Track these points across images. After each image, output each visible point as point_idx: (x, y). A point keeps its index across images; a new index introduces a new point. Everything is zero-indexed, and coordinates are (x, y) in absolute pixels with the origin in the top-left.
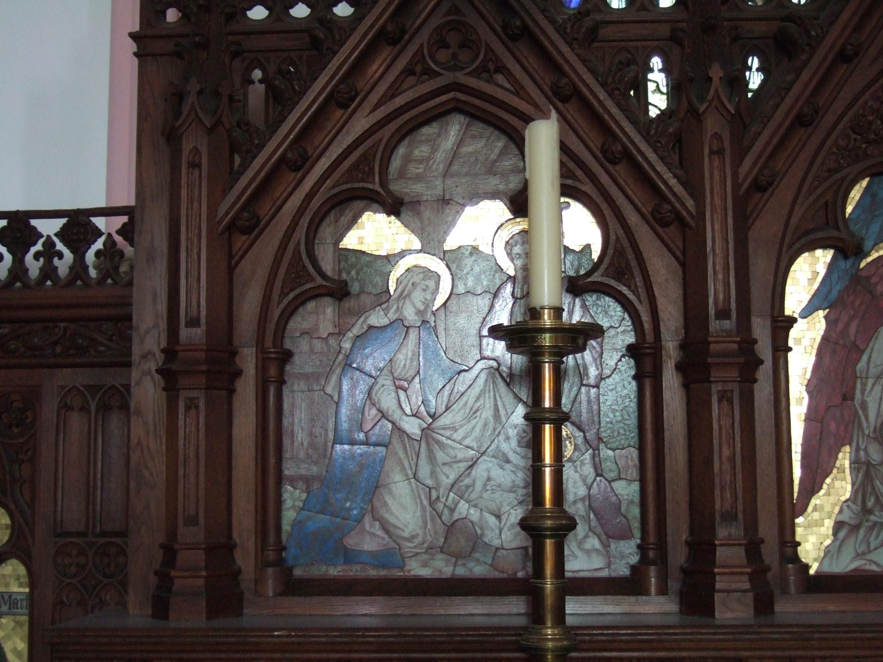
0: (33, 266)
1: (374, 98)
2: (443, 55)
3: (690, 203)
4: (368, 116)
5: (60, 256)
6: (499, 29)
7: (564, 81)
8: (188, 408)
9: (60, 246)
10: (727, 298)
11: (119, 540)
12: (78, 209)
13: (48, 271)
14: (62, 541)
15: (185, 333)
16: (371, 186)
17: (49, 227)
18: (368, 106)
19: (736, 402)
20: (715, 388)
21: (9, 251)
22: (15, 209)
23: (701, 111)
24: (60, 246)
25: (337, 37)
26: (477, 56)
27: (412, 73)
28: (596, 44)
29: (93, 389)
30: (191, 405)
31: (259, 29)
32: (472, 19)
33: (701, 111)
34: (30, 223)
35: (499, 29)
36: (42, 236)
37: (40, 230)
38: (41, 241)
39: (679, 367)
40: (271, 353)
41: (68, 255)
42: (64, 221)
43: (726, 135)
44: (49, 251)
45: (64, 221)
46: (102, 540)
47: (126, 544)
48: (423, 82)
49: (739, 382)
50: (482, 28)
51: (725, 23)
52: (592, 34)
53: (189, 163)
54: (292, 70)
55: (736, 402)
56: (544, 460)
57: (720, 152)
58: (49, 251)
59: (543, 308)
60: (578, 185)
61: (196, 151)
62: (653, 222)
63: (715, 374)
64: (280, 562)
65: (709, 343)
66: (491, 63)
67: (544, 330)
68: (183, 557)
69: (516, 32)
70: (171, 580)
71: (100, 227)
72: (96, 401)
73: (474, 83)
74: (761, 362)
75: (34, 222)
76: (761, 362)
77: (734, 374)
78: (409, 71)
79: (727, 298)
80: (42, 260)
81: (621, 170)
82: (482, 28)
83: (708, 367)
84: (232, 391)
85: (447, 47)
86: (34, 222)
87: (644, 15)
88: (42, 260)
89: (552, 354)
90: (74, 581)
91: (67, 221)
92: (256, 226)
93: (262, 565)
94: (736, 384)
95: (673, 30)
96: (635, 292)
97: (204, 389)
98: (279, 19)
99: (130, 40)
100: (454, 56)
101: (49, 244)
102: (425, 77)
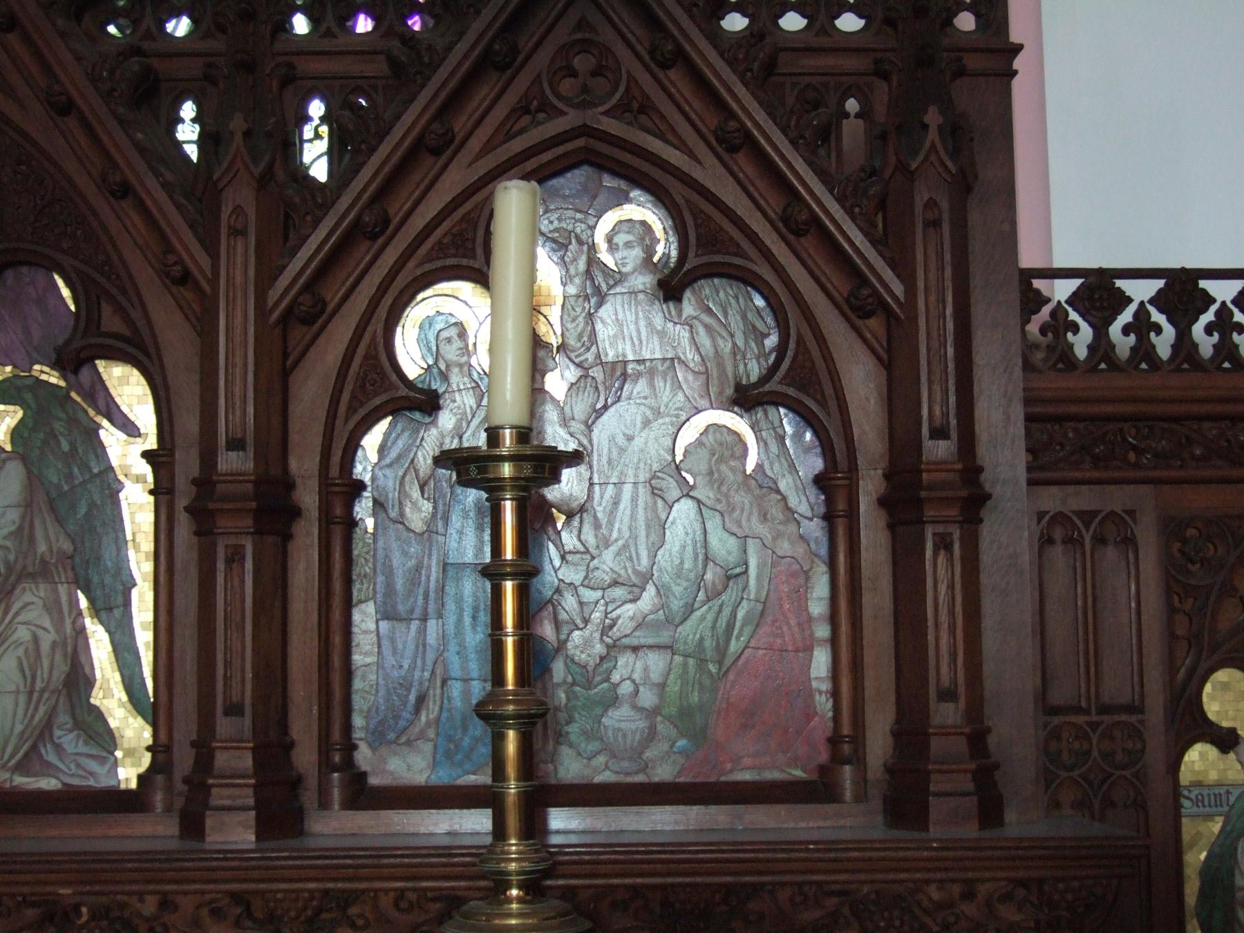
0: (1123, 343)
1: (475, 144)
2: (567, 86)
3: (898, 288)
4: (470, 164)
5: (1158, 329)
6: (643, 52)
7: (733, 124)
8: (229, 561)
9: (1157, 317)
10: (946, 415)
11: (1133, 719)
12: (1183, 270)
13: (1143, 350)
14: (1056, 720)
15: (229, 462)
16: (471, 263)
17: (1141, 291)
18: (464, 157)
19: (957, 547)
20: (929, 532)
21: (1170, 320)
22: (1179, 267)
23: (914, 165)
24: (1157, 317)
25: (426, 60)
26: (616, 89)
27: (526, 111)
28: (774, 79)
29: (1087, 516)
30: (235, 557)
31: (303, 47)
32: (607, 35)
33: (914, 165)
34: (1031, 284)
35: (643, 52)
36: (1214, 301)
37: (1212, 293)
38: (1214, 308)
39: (295, 513)
40: (336, 485)
41: (1086, 331)
42: (1160, 283)
43: (945, 205)
44: (1141, 326)
45: (1160, 283)
46: (1107, 719)
47: (1141, 722)
48: (540, 124)
49: (959, 522)
50: (622, 51)
51: (945, 54)
52: (770, 67)
53: (230, 227)
54: (364, 103)
55: (957, 547)
56: (506, 627)
57: (936, 224)
58: (1141, 326)
59: (503, 428)
60: (749, 265)
61: (238, 210)
62: (849, 312)
63: (929, 513)
64: (348, 763)
65: (921, 471)
66: (635, 102)
67: (502, 459)
68: (222, 760)
69: (667, 56)
70: (207, 789)
71: (1235, 293)
72: (1091, 533)
73: (613, 126)
74: (187, 509)
75: (1120, 283)
76: (187, 509)
77: (954, 512)
78: (523, 109)
79: (946, 415)
80: (1216, 335)
81: (809, 244)
82: (622, 51)
83: (919, 503)
84: (287, 537)
85: (574, 74)
86: (1120, 283)
87: (823, 41)
88: (1216, 335)
89: (514, 488)
90: (1127, 773)
91: (1166, 284)
92: (322, 312)
93: (325, 765)
94: (250, 538)
95: (877, 62)
96: (823, 404)
97: (959, 522)
98: (329, 34)
99: (1019, 42)
100: (585, 89)
101: (1142, 312)
102: (541, 116)
